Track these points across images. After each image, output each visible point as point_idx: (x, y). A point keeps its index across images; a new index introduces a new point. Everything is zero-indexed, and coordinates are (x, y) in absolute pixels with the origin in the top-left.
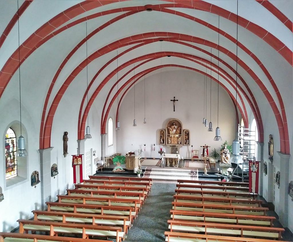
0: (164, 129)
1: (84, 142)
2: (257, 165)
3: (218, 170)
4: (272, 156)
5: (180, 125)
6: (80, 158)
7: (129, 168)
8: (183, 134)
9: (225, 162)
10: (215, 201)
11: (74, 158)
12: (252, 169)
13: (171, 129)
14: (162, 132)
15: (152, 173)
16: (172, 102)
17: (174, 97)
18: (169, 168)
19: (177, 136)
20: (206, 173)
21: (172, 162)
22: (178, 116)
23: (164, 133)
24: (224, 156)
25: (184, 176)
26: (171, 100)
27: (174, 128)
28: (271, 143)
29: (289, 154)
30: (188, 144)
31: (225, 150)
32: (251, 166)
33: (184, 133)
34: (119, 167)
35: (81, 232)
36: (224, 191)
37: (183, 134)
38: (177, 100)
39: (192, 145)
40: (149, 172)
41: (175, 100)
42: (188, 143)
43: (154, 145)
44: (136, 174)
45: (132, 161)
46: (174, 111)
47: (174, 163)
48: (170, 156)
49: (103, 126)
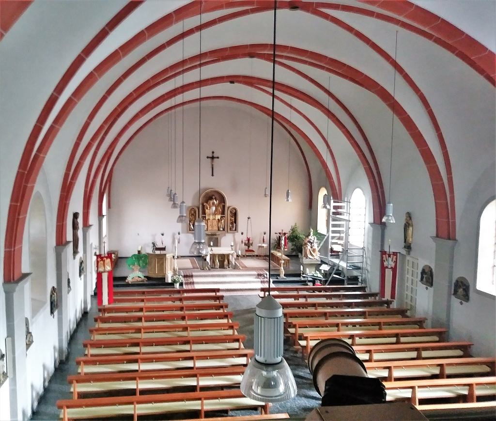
0: (197, 207)
3: (302, 269)
5: (222, 199)
7: (156, 273)
8: (228, 213)
9: (310, 257)
10: (126, 321)
11: (99, 259)
12: (386, 264)
13: (208, 207)
14: (193, 212)
15: (195, 280)
16: (209, 160)
17: (213, 152)
18: (219, 271)
19: (218, 217)
20: (282, 275)
21: (224, 261)
22: (217, 183)
23: (195, 212)
24: (309, 247)
25: (250, 282)
27: (213, 204)
28: (409, 224)
29: (454, 239)
30: (236, 230)
31: (310, 237)
32: (384, 259)
33: (229, 212)
34: (134, 275)
35: (134, 387)
36: (215, 303)
37: (228, 213)
38: (218, 158)
39: (242, 231)
40: (190, 280)
41: (215, 158)
42: (234, 229)
43: (179, 234)
44: (172, 284)
45: (161, 262)
46: (213, 175)
47: (226, 262)
48: (220, 251)
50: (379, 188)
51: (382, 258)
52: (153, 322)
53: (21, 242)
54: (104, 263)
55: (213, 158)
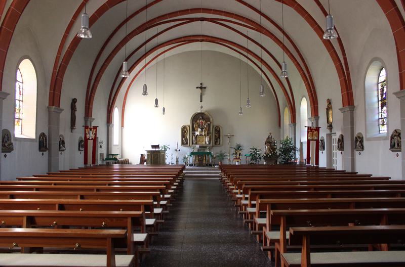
1: (59, 116)
2: (95, 130)
4: (331, 123)
6: (316, 132)
12: (88, 136)
16: (199, 89)
26: (197, 88)
32: (87, 132)
49: (89, 104)
50: (311, 87)
51: (85, 131)
52: (196, 17)
53: (309, 96)
54: (313, 134)
55: (201, 88)
